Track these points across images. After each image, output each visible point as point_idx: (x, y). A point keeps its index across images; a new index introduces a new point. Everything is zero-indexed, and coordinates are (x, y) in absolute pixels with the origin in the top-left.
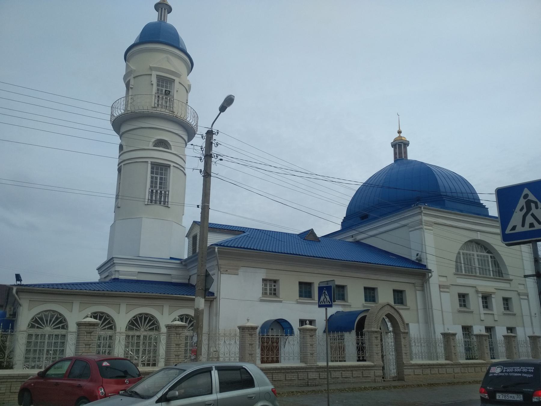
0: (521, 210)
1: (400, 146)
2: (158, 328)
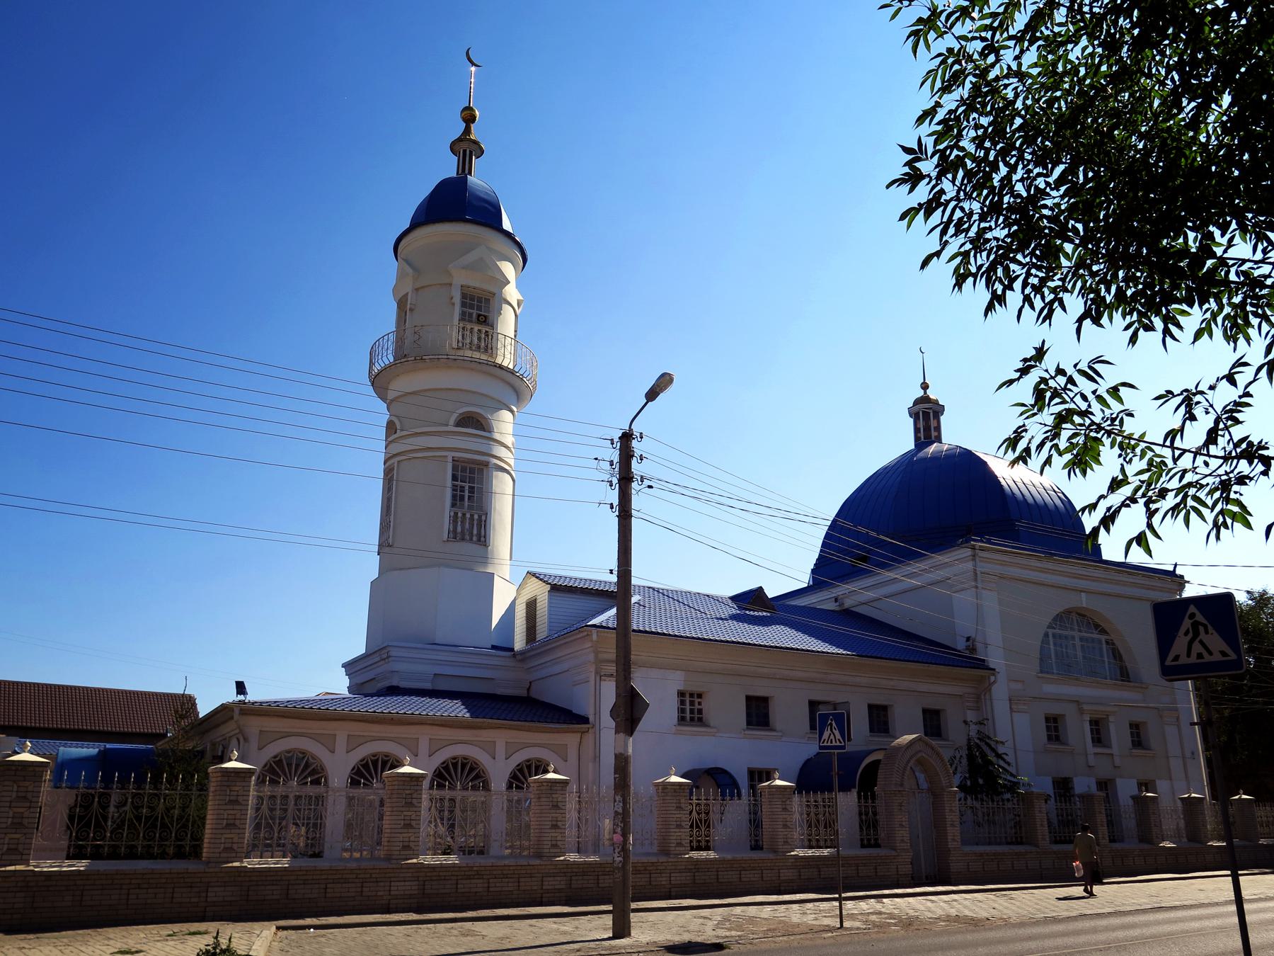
0: (1186, 633)
1: (926, 415)
2: (486, 787)
